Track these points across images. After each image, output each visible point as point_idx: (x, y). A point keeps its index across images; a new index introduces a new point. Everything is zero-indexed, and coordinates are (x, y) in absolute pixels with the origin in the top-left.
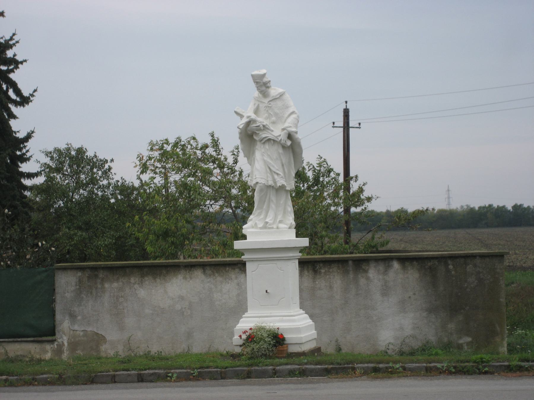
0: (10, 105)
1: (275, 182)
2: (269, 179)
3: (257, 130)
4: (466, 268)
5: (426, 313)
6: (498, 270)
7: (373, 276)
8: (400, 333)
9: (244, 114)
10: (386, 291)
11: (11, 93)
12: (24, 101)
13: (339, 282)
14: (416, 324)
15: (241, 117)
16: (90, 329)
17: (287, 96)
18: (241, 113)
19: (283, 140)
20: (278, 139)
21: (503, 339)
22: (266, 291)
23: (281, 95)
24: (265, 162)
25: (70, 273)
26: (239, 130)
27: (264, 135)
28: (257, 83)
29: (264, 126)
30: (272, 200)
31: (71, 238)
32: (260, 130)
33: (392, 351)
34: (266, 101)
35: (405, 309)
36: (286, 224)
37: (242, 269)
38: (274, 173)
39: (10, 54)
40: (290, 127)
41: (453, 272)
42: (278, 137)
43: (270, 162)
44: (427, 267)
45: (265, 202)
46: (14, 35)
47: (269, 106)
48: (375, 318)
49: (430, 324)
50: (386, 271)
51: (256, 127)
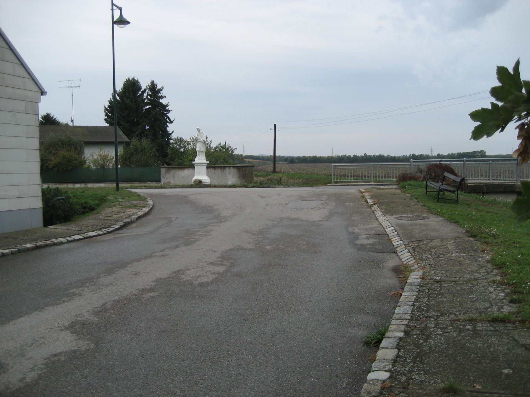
0: (167, 123)
10: (230, 173)
11: (167, 119)
12: (171, 122)
13: (220, 171)
16: (167, 180)
17: (204, 132)
23: (203, 132)
25: (164, 168)
27: (199, 140)
28: (197, 130)
31: (178, 162)
34: (199, 133)
39: (167, 108)
46: (169, 103)
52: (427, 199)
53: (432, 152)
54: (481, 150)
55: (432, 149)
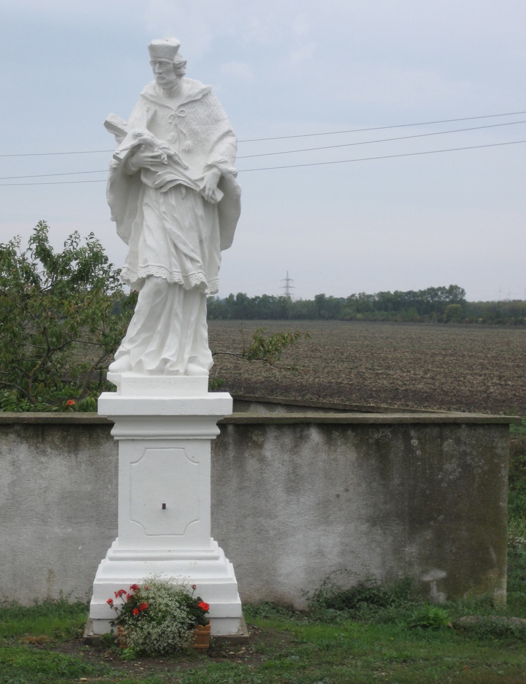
1: (186, 277)
2: (175, 270)
3: (151, 165)
4: (441, 445)
5: (366, 525)
6: (498, 451)
7: (272, 456)
8: (318, 561)
9: (126, 130)
14: (347, 545)
15: (117, 136)
17: (213, 98)
18: (120, 127)
19: (210, 189)
20: (197, 186)
21: (500, 575)
22: (164, 506)
23: (206, 94)
24: (165, 231)
26: (114, 161)
29: (170, 157)
30: (177, 315)
32: (162, 165)
33: (302, 593)
34: (174, 104)
35: (329, 516)
36: (202, 365)
37: (23, 435)
38: (184, 258)
40: (225, 162)
41: (418, 452)
42: (199, 183)
43: (179, 233)
44: (371, 441)
45: (159, 317)
47: (180, 115)
48: (272, 533)
49: (374, 546)
50: (296, 446)
51: (152, 157)
52: (338, 436)
53: (287, 287)
54: (451, 287)
55: (288, 280)
